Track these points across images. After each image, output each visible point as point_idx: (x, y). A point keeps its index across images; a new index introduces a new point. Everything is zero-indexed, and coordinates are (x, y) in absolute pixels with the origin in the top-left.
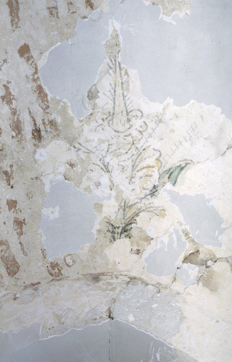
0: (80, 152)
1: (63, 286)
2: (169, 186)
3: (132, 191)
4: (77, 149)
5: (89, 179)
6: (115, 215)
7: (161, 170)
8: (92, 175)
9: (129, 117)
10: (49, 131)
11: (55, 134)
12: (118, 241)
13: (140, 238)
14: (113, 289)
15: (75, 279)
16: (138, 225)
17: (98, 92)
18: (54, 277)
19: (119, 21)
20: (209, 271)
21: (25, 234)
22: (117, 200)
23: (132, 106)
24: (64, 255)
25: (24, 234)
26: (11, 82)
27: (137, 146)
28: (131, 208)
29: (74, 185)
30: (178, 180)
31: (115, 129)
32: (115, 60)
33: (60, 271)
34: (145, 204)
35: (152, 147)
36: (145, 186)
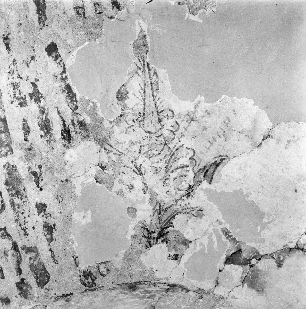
0: (111, 154)
1: (97, 295)
2: (205, 184)
3: (166, 193)
4: (107, 151)
5: (121, 182)
6: (150, 219)
7: (195, 169)
8: (124, 177)
9: (160, 117)
10: (79, 132)
11: (85, 135)
12: (154, 247)
13: (178, 242)
14: (152, 297)
15: (110, 288)
16: (175, 229)
17: (128, 93)
18: (88, 288)
19: (146, 21)
20: (254, 271)
21: (55, 240)
22: (151, 203)
23: (163, 106)
24: (97, 263)
25: (54, 240)
26: (39, 80)
27: (170, 146)
28: (166, 211)
29: (106, 189)
30: (214, 177)
31: (146, 130)
32: (143, 61)
33: (93, 280)
34: (181, 205)
35: (185, 147)
36: (180, 187)
